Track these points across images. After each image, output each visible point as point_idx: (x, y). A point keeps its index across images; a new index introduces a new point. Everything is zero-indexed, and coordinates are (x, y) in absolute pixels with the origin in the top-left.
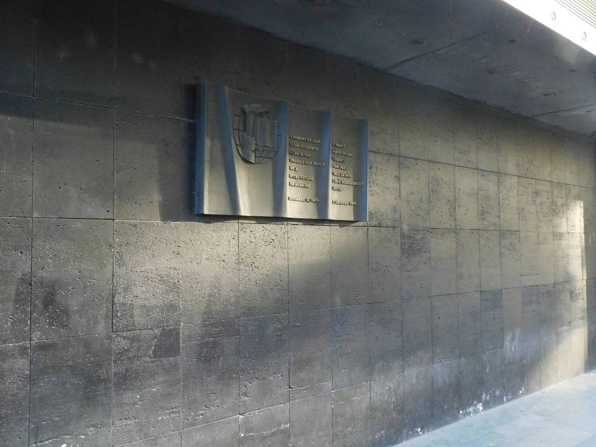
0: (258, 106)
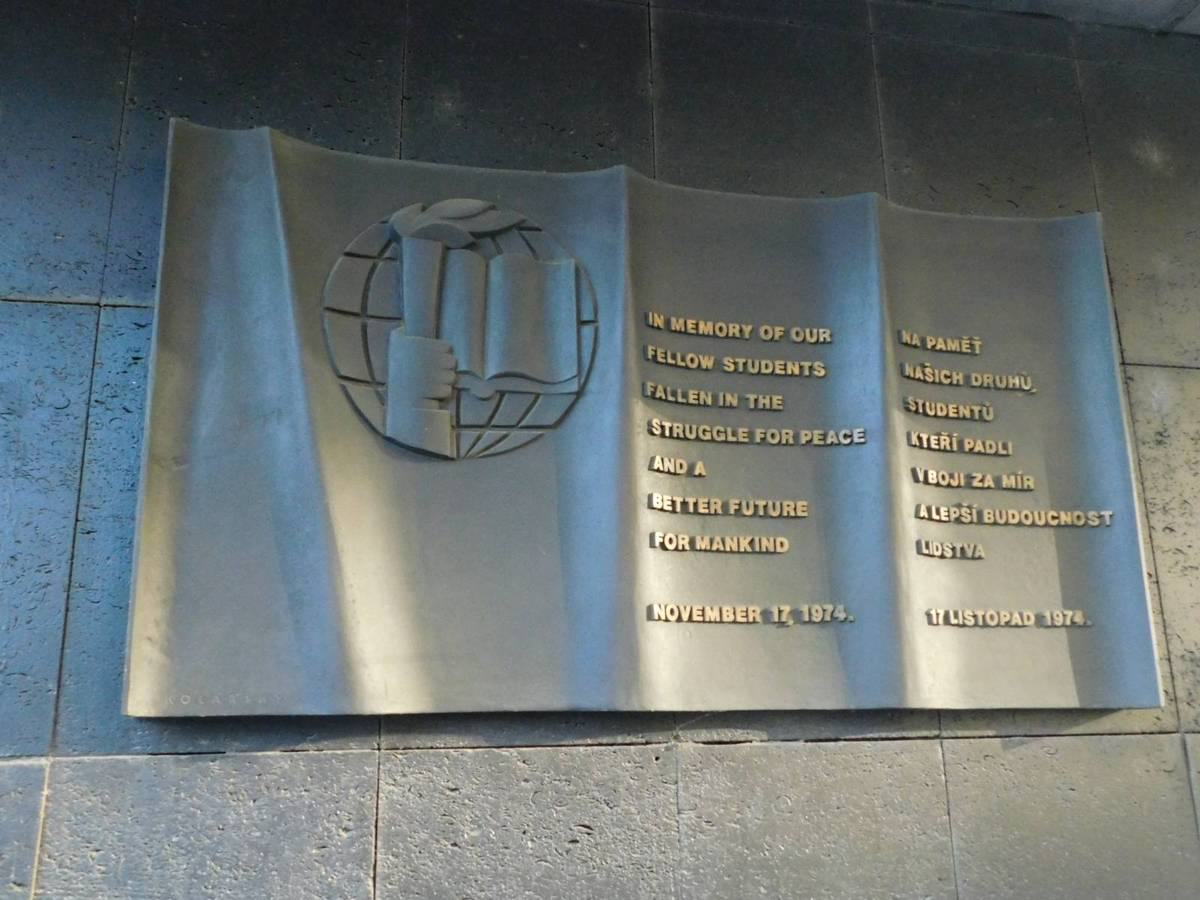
0: (473, 204)
